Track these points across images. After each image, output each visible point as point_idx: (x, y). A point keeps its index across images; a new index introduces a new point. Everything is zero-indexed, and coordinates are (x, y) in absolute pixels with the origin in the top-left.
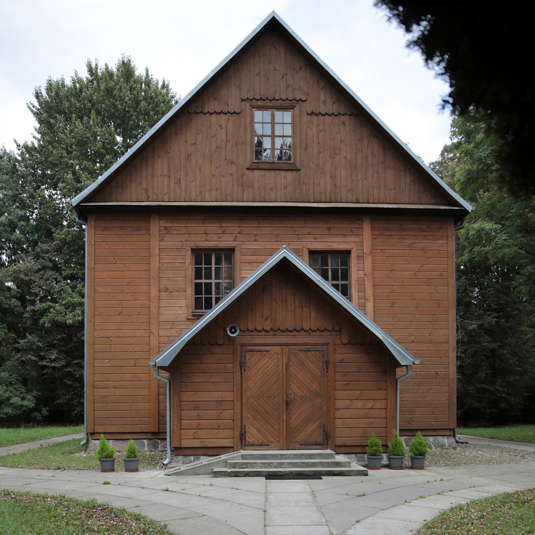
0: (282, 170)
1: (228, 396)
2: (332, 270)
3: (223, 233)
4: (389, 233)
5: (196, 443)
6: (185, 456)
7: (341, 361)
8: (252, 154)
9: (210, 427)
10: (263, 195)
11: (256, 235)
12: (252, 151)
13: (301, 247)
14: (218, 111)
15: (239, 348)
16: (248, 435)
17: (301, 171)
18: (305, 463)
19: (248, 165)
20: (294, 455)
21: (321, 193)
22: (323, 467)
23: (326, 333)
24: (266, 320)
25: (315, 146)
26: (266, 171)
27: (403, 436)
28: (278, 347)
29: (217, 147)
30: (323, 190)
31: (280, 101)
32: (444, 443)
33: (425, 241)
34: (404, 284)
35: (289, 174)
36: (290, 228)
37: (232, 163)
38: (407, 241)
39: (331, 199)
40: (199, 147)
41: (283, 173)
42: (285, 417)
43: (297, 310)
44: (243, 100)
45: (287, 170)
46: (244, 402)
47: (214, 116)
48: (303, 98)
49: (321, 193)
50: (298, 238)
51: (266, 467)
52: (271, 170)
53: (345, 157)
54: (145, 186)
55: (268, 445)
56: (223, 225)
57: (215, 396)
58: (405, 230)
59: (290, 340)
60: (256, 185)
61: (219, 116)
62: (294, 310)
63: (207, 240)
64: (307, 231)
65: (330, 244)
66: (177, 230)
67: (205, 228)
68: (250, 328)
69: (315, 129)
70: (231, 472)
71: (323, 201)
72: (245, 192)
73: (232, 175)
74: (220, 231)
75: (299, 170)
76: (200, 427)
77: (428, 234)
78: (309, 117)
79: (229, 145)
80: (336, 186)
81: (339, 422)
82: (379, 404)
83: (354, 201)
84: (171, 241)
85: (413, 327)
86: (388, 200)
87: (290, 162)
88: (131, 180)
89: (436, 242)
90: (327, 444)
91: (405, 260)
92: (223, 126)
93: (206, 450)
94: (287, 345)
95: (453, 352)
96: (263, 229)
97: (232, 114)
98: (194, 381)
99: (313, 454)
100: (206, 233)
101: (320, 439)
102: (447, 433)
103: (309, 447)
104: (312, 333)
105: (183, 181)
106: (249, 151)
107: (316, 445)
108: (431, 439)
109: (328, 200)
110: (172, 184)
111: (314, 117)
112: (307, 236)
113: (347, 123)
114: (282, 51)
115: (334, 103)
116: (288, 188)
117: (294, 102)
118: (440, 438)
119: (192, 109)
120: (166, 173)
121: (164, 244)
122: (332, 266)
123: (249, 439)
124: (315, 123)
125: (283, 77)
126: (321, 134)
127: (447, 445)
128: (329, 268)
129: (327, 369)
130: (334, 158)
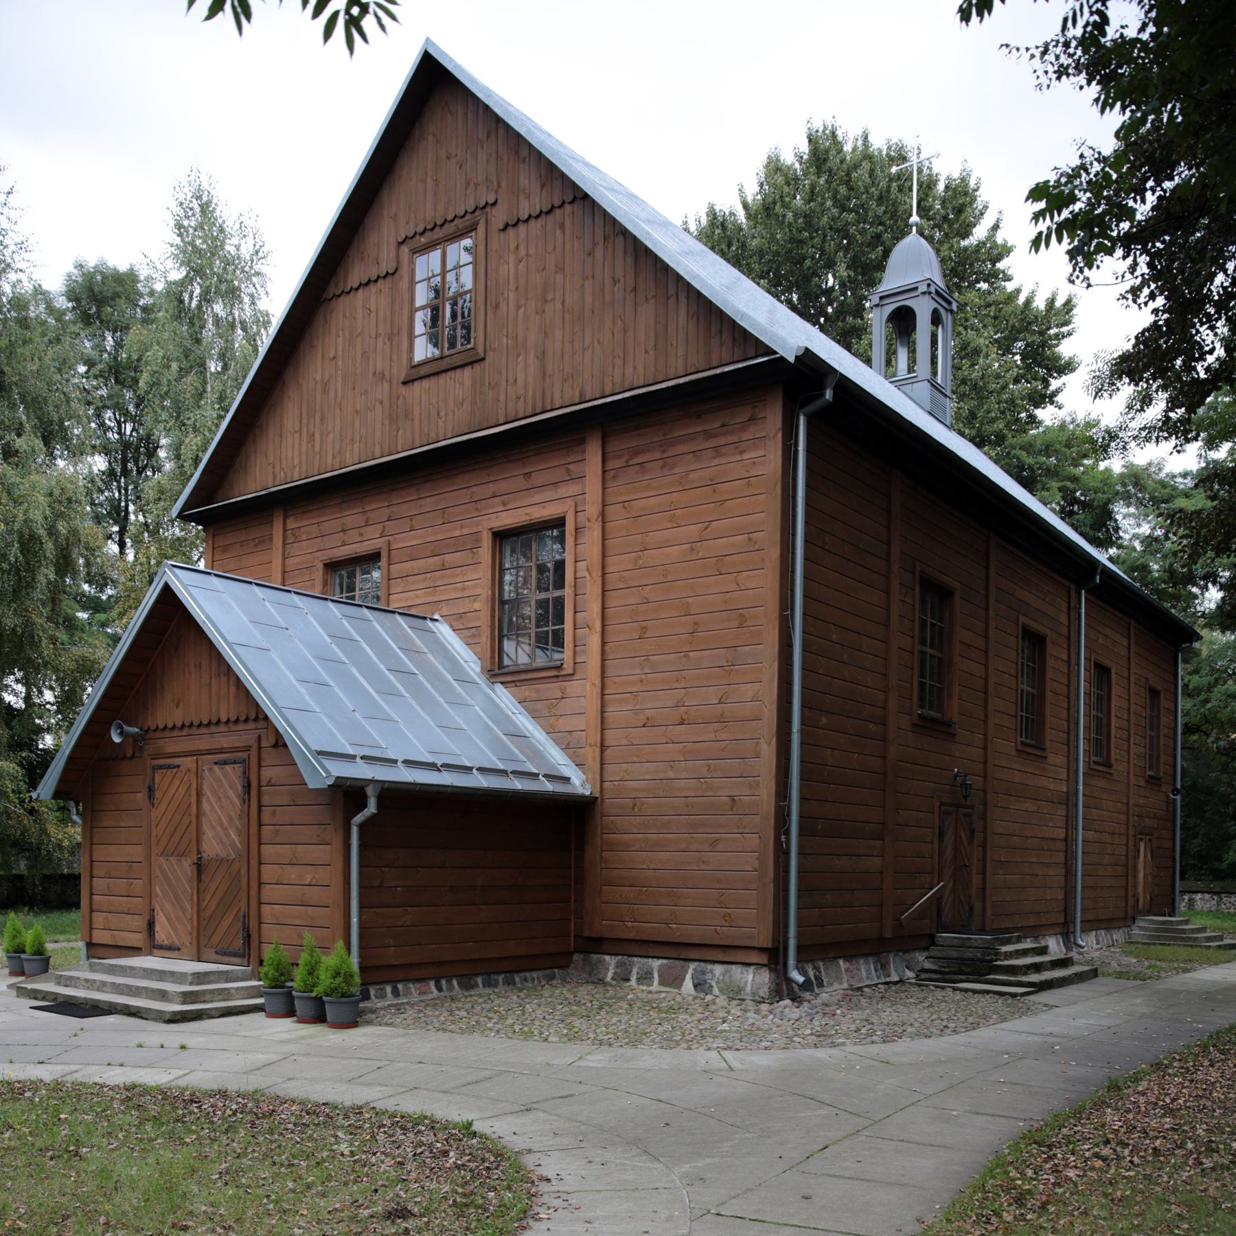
13: (480, 529)
14: (365, 281)
17: (487, 361)
24: (177, 706)
26: (432, 378)
27: (659, 958)
33: (717, 462)
36: (464, 491)
38: (676, 470)
39: (534, 407)
40: (340, 363)
45: (463, 366)
50: (477, 509)
54: (271, 458)
55: (179, 949)
56: (367, 508)
58: (674, 443)
61: (367, 289)
64: (491, 488)
65: (528, 510)
72: (400, 433)
73: (381, 402)
78: (502, 233)
80: (544, 374)
85: (682, 685)
88: (255, 452)
89: (738, 458)
91: (671, 519)
92: (373, 308)
98: (105, 824)
100: (343, 531)
101: (239, 943)
102: (754, 957)
103: (226, 959)
105: (317, 436)
108: (718, 969)
115: (543, 186)
118: (736, 970)
123: (161, 936)
124: (512, 247)
127: (748, 989)
129: (249, 800)
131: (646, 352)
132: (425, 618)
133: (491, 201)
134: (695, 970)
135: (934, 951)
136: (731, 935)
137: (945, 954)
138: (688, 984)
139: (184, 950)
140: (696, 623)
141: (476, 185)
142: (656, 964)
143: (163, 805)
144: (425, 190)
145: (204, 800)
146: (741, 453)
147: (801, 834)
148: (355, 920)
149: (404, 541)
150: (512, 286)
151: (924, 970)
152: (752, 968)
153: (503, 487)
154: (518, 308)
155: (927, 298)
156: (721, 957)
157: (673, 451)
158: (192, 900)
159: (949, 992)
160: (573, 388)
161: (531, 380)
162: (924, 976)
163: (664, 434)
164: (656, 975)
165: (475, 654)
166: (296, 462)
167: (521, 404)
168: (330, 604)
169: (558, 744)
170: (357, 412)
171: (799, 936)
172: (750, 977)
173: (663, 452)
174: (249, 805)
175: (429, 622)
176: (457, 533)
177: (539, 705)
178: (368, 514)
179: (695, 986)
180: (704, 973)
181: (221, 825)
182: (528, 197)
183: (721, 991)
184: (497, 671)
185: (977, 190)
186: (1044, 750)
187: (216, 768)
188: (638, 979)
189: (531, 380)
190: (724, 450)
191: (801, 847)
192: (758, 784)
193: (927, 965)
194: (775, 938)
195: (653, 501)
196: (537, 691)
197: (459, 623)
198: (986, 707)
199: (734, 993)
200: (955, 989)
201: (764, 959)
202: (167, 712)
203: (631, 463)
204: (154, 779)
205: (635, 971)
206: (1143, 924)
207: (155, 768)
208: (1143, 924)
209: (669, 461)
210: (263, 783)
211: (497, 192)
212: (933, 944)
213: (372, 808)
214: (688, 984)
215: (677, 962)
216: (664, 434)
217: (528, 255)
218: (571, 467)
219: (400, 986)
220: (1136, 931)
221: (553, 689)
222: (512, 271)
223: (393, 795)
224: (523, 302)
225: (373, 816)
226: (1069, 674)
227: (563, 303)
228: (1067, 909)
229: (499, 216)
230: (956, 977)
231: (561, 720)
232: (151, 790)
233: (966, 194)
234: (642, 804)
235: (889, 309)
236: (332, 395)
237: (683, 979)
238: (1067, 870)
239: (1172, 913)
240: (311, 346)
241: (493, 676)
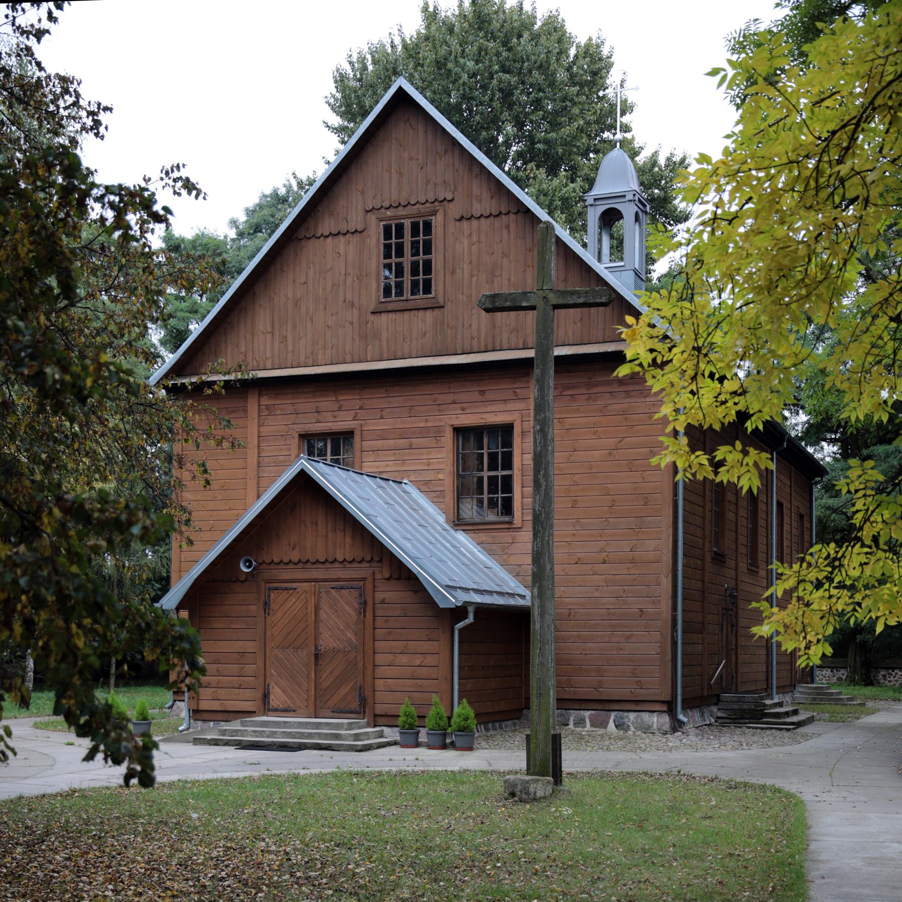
0: (418, 309)
1: (250, 646)
2: (489, 454)
3: (340, 409)
4: (570, 392)
5: (215, 706)
6: (204, 721)
7: (383, 602)
8: (378, 290)
9: (231, 685)
10: (393, 349)
11: (382, 410)
12: (379, 285)
13: (443, 424)
14: (334, 232)
15: (263, 585)
16: (272, 697)
17: (446, 308)
18: (300, 733)
19: (372, 308)
20: (299, 723)
21: (472, 338)
22: (320, 739)
23: (365, 565)
24: (293, 548)
25: (466, 267)
26: (398, 313)
27: (588, 710)
28: (307, 584)
29: (334, 285)
30: (475, 334)
31: (417, 206)
32: (650, 723)
33: (627, 400)
34: (593, 471)
35: (429, 313)
36: (429, 396)
37: (352, 305)
38: (598, 403)
39: (486, 346)
40: (311, 288)
41: (421, 313)
42: (313, 676)
43: (330, 534)
44: (367, 211)
45: (425, 309)
46: (267, 655)
47: (330, 239)
48: (449, 197)
49: (472, 338)
50: (440, 411)
51: (257, 736)
52: (403, 310)
53: (509, 280)
54: (243, 350)
55: (294, 711)
56: (340, 398)
57: (237, 646)
58: (596, 385)
59: (320, 573)
60: (384, 335)
61: (336, 239)
62: (326, 536)
63: (318, 422)
64: (451, 397)
65: (484, 416)
66: (282, 410)
67: (317, 404)
68: (276, 560)
69: (466, 242)
70: (211, 739)
71: (475, 350)
72: (369, 347)
73: (352, 323)
74: (335, 406)
75: (443, 307)
76: (220, 685)
77: (630, 388)
78: (458, 223)
79: (349, 280)
80: (494, 326)
81: (379, 683)
82: (429, 660)
83: (521, 346)
84: (275, 425)
85: (604, 539)
86: (571, 339)
87: (430, 296)
88: (226, 342)
89: (643, 400)
90: (364, 712)
91: (595, 433)
92: (342, 253)
93: (227, 714)
94: (316, 580)
95: (667, 577)
96: (391, 399)
97: (353, 233)
98: (214, 626)
99: (321, 723)
100: (317, 412)
101: (355, 705)
102: (658, 707)
103: (342, 715)
104: (348, 565)
105: (290, 339)
106: (374, 285)
107: (351, 712)
108: (632, 716)
109: (483, 349)
110: (277, 343)
111: (465, 224)
112: (451, 406)
113: (512, 226)
114: (421, 128)
115: (492, 198)
116: (427, 336)
117: (436, 204)
118: (645, 716)
119: (302, 233)
120: (269, 330)
121: (265, 430)
122: (489, 449)
123: (274, 702)
124: (466, 233)
125: (422, 168)
126: (474, 248)
127: (655, 726)
128: (485, 451)
129: (365, 612)
130: (493, 282)
131: (575, 323)
132: (388, 480)
133: (449, 198)
134: (616, 716)
135: (721, 705)
136: (643, 694)
137: (729, 707)
138: (611, 725)
139: (299, 711)
140: (614, 501)
141: (435, 184)
142: (587, 714)
143: (279, 615)
144: (390, 177)
145: (321, 612)
146: (645, 397)
147: (684, 632)
148: (456, 687)
149: (375, 425)
150: (466, 259)
151: (718, 718)
152: (656, 714)
153: (462, 397)
154: (472, 276)
155: (632, 204)
156: (635, 708)
157: (595, 390)
158: (308, 676)
159: (744, 729)
160: (518, 338)
161: (483, 327)
162: (720, 721)
163: (589, 378)
164: (588, 721)
165: (440, 509)
166: (268, 355)
167: (475, 342)
168: (351, 473)
169: (510, 573)
170: (328, 327)
171: (683, 694)
172: (655, 719)
173: (588, 389)
174: (365, 616)
175: (403, 485)
176: (422, 425)
177: (494, 547)
178: (341, 403)
179: (616, 727)
180: (622, 718)
181: (339, 629)
182: (480, 201)
183: (636, 728)
184: (457, 522)
185: (610, 57)
186: (757, 567)
187: (333, 591)
188: (575, 724)
189: (483, 327)
190: (632, 394)
191: (683, 639)
192: (659, 601)
193: (720, 714)
194: (672, 697)
195: (580, 420)
196: (493, 537)
197: (425, 486)
198: (736, 542)
199: (647, 729)
200: (748, 728)
201: (665, 708)
202: (281, 551)
203: (565, 393)
204: (269, 597)
205: (572, 719)
206: (801, 690)
207: (270, 589)
208: (801, 690)
209: (593, 396)
210: (377, 602)
211: (453, 193)
212: (719, 701)
213: (470, 619)
214: (611, 725)
215: (602, 712)
216: (589, 378)
217: (479, 242)
218: (517, 391)
219: (497, 724)
220: (797, 695)
221: (506, 536)
222: (466, 249)
223: (482, 611)
224: (475, 273)
225: (471, 624)
226: (767, 512)
227: (509, 280)
228: (768, 679)
229: (455, 210)
230: (742, 721)
231: (512, 557)
232: (266, 604)
233: (600, 59)
234: (576, 613)
235: (601, 209)
236: (303, 310)
237: (608, 723)
238: (768, 651)
239: (812, 682)
240: (282, 270)
241: (456, 525)
